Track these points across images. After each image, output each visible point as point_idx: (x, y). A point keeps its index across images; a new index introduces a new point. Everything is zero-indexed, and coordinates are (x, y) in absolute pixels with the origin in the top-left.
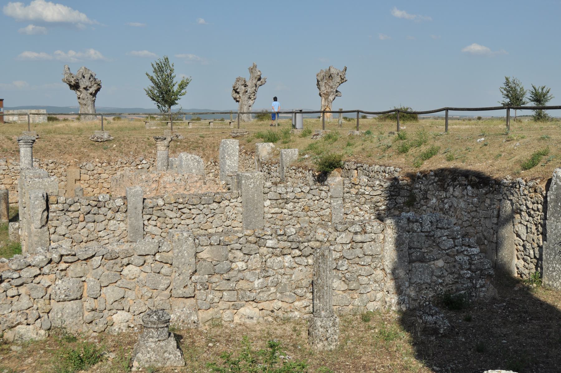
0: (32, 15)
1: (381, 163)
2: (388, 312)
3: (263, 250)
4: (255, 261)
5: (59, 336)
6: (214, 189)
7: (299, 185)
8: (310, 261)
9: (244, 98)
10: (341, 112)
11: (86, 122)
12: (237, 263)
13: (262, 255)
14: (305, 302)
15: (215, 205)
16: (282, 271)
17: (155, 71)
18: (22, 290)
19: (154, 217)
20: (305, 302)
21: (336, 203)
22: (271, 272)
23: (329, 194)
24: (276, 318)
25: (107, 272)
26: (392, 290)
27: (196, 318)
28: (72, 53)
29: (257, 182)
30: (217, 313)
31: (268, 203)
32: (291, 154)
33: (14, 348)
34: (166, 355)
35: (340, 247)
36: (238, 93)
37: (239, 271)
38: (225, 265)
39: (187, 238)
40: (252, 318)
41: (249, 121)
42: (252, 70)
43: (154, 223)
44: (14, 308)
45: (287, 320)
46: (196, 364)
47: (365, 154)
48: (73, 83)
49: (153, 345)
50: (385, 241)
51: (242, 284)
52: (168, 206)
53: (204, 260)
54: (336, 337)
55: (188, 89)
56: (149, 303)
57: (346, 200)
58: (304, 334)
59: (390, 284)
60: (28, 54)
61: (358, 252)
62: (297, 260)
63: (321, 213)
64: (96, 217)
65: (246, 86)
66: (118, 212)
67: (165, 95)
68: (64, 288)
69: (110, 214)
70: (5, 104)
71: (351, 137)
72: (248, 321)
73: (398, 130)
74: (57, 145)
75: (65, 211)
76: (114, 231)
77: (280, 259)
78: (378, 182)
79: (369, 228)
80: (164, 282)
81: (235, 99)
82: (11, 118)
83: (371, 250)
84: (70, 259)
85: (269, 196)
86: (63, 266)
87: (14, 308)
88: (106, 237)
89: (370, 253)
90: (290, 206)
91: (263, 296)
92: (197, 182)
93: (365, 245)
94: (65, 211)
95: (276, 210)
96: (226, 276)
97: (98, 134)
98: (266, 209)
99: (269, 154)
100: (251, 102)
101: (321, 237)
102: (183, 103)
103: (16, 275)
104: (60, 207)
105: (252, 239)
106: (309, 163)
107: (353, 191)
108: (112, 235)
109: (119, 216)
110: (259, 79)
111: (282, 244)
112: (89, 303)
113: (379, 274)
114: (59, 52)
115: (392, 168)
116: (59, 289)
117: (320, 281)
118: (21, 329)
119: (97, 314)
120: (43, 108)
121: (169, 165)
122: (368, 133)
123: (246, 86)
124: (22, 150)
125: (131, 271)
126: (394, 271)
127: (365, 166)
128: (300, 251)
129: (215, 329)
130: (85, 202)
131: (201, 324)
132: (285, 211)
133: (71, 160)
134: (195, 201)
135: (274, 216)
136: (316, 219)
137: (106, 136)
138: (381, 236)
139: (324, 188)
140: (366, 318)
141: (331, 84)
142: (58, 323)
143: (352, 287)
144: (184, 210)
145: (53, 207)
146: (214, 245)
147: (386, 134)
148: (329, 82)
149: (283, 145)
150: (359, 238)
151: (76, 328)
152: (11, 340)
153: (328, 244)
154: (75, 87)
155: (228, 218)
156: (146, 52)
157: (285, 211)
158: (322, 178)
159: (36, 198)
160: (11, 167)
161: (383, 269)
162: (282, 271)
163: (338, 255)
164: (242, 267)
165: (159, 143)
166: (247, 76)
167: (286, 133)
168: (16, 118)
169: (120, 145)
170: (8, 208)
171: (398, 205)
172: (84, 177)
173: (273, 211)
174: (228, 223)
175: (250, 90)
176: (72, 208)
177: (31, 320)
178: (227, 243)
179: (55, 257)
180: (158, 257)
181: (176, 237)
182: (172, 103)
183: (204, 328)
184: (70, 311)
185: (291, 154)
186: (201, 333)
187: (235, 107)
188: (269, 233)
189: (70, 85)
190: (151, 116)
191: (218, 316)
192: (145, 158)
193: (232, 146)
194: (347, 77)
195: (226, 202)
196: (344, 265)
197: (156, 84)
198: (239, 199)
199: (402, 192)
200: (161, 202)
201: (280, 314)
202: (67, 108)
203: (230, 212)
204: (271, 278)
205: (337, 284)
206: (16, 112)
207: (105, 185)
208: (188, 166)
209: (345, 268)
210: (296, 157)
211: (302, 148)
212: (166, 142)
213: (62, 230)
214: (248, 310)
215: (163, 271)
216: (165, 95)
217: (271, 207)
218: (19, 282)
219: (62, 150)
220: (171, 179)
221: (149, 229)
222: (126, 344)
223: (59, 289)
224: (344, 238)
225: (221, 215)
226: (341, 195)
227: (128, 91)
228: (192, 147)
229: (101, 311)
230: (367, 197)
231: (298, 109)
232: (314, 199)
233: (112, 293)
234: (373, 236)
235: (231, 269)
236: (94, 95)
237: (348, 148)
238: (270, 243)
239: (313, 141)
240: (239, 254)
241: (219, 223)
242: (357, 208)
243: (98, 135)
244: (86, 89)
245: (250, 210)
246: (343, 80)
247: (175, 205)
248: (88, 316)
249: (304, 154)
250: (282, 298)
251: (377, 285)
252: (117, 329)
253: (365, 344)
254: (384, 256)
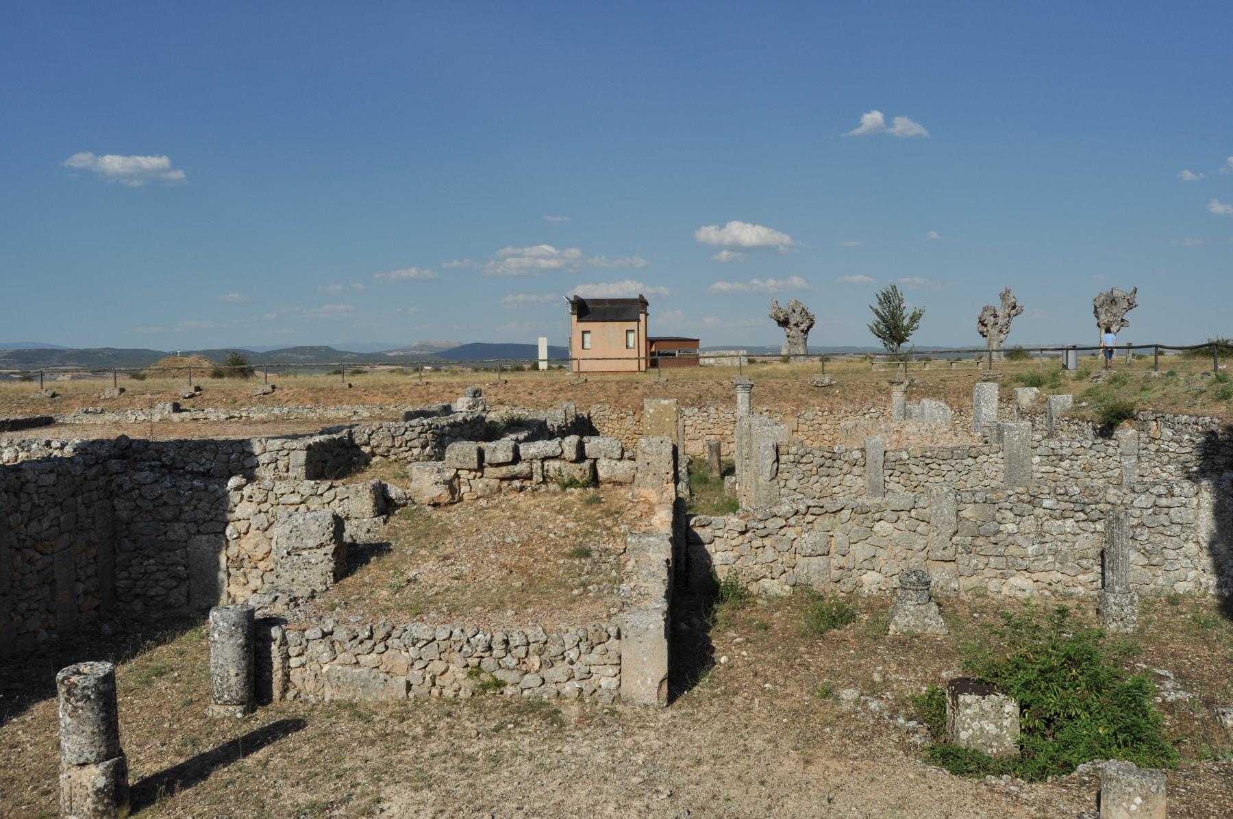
0: (727, 240)
1: (1191, 412)
2: (1204, 596)
3: (1039, 511)
4: (1028, 524)
5: (804, 594)
6: (968, 442)
7: (1077, 439)
8: (1100, 526)
9: (993, 332)
10: (1129, 347)
11: (797, 365)
13: (1037, 517)
14: (1091, 576)
15: (970, 461)
16: (1063, 537)
17: (881, 303)
18: (767, 542)
19: (897, 473)
20: (1091, 576)
21: (1128, 462)
22: (1048, 538)
23: (1119, 450)
24: (1054, 593)
25: (856, 528)
26: (1209, 569)
28: (771, 282)
30: (982, 581)
31: (1037, 459)
32: (1063, 401)
33: (759, 601)
34: (927, 620)
35: (1138, 512)
36: (986, 326)
37: (1009, 534)
38: (992, 526)
39: (947, 494)
41: (1000, 359)
42: (1004, 297)
43: (897, 479)
44: (759, 560)
45: (1068, 596)
46: (961, 634)
47: (1167, 401)
48: (782, 318)
49: (912, 608)
50: (1199, 508)
51: (1012, 550)
52: (913, 461)
53: (967, 520)
54: (1135, 618)
55: (921, 322)
56: (903, 565)
58: (1091, 613)
59: (1206, 561)
60: (722, 286)
61: (1162, 518)
62: (1081, 525)
63: (1107, 474)
64: (831, 470)
65: (995, 316)
67: (893, 329)
69: (846, 467)
70: (702, 345)
71: (1147, 379)
72: (1020, 594)
73: (1216, 369)
74: (772, 391)
75: (796, 463)
76: (851, 486)
77: (1060, 522)
78: (1187, 437)
79: (1177, 490)
80: (920, 543)
81: (981, 333)
82: (707, 361)
84: (817, 511)
85: (1038, 451)
86: (810, 518)
87: (759, 560)
90: (1066, 464)
91: (1039, 565)
93: (1172, 511)
94: (796, 463)
95: (1048, 468)
96: (993, 539)
97: (818, 378)
98: (1035, 468)
99: (1032, 401)
100: (1002, 337)
101: (1113, 499)
102: (916, 340)
103: (761, 526)
104: (791, 458)
105: (1025, 497)
106: (1088, 413)
107: (1153, 447)
109: (857, 470)
110: (1014, 308)
111: (1063, 505)
112: (837, 561)
113: (1191, 548)
114: (755, 281)
115: (1208, 419)
117: (1113, 549)
118: (766, 583)
119: (845, 572)
120: (743, 348)
121: (906, 414)
122: (1172, 374)
123: (995, 316)
124: (740, 396)
125: (883, 527)
126: (1211, 546)
127: (1168, 416)
129: (978, 600)
130: (818, 454)
131: (962, 593)
132: (1059, 470)
133: (788, 408)
134: (946, 455)
137: (827, 380)
138: (1195, 501)
139: (1112, 443)
140: (1173, 600)
141: (1115, 311)
142: (803, 579)
143: (1154, 562)
144: (932, 466)
145: (783, 458)
147: (1198, 376)
148: (1111, 309)
149: (1051, 391)
150: (1164, 502)
151: (822, 586)
152: (755, 593)
153: (1122, 507)
154: (784, 323)
155: (986, 477)
156: (861, 277)
157: (1059, 470)
158: (1106, 430)
159: (766, 448)
160: (722, 415)
161: (1197, 542)
162: (1063, 537)
163: (1136, 522)
165: (894, 388)
166: (997, 304)
167: (1055, 375)
168: (712, 361)
169: (844, 391)
170: (720, 461)
172: (802, 427)
173: (1044, 469)
174: (986, 482)
175: (1001, 321)
176: (804, 460)
177: (775, 574)
179: (802, 508)
180: (913, 513)
181: (934, 492)
182: (901, 340)
183: (966, 597)
185: (1063, 401)
186: (963, 602)
187: (981, 343)
188: (1047, 491)
189: (779, 322)
190: (868, 356)
191: (983, 585)
192: (874, 406)
193: (990, 392)
194: (1137, 301)
195: (984, 458)
196: (1144, 535)
197: (881, 317)
198: (1001, 455)
199: (1222, 450)
200: (905, 456)
201: (1060, 588)
202: (764, 348)
203: (989, 469)
204: (1048, 545)
205: (1134, 556)
206: (712, 354)
207: (826, 437)
208: (931, 414)
209: (1144, 538)
210: (1069, 405)
211: (1077, 394)
212: (903, 387)
213: (793, 483)
214: (1019, 581)
215: (919, 529)
216: (893, 329)
217: (1041, 464)
218: (765, 532)
219: (777, 396)
220: (915, 429)
221: (891, 486)
222: (881, 608)
224: (1143, 501)
226: (1136, 451)
227: (848, 326)
228: (934, 392)
229: (850, 570)
230: (1172, 455)
231: (1070, 344)
234: (1183, 500)
235: (999, 532)
236: (806, 332)
237: (1143, 393)
238: (1047, 503)
239: (1092, 385)
240: (1010, 515)
241: (975, 481)
242: (1157, 469)
243: (818, 379)
244: (796, 325)
245: (1015, 467)
246: (1131, 305)
248: (836, 574)
249: (1080, 402)
253: (1173, 630)
254: (1198, 526)
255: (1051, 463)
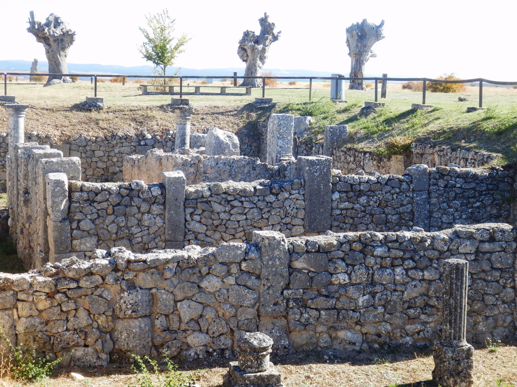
4: (360, 275)
12: (339, 275)
27: (287, 343)
29: (324, 169)
38: (323, 277)
40: (354, 344)
44: (70, 325)
57: (433, 195)
63: (401, 209)
66: (154, 203)
68: (131, 302)
69: (144, 207)
83: (501, 262)
88: (139, 235)
89: (499, 265)
90: (363, 200)
92: (245, 167)
98: (335, 204)
107: (442, 183)
108: (146, 232)
109: (156, 209)
116: (125, 302)
125: (211, 284)
128: (415, 262)
132: (357, 206)
135: (344, 212)
136: (394, 217)
146: (311, 252)
157: (357, 206)
164: (345, 280)
171: (496, 202)
173: (342, 206)
174: (288, 220)
178: (327, 250)
184: (138, 330)
207: (100, 164)
217: (341, 199)
223: (125, 302)
225: (279, 210)
232: (393, 191)
233: (189, 309)
247: (223, 196)
250: (391, 319)
251: (507, 306)
252: (193, 354)
255: (348, 200)
